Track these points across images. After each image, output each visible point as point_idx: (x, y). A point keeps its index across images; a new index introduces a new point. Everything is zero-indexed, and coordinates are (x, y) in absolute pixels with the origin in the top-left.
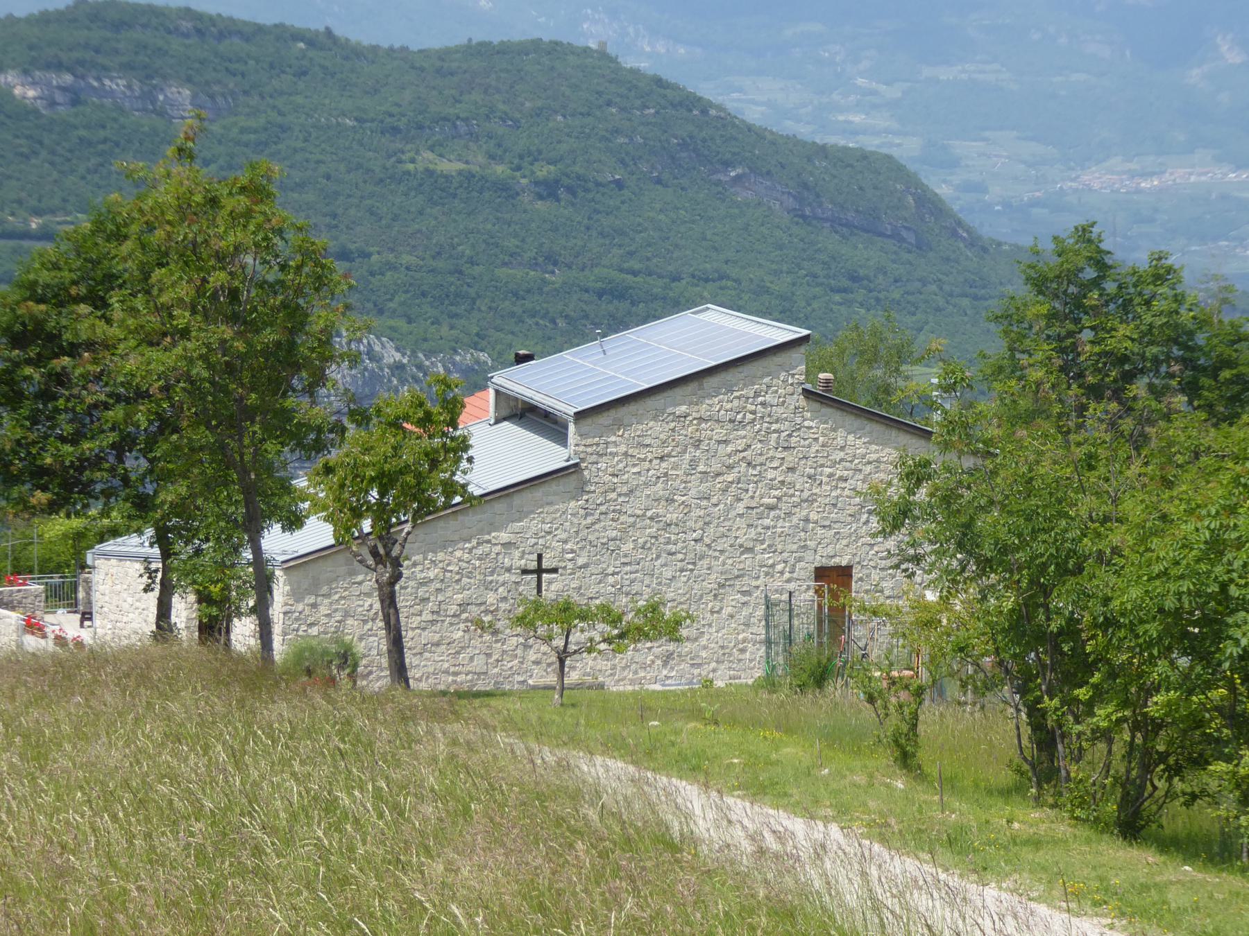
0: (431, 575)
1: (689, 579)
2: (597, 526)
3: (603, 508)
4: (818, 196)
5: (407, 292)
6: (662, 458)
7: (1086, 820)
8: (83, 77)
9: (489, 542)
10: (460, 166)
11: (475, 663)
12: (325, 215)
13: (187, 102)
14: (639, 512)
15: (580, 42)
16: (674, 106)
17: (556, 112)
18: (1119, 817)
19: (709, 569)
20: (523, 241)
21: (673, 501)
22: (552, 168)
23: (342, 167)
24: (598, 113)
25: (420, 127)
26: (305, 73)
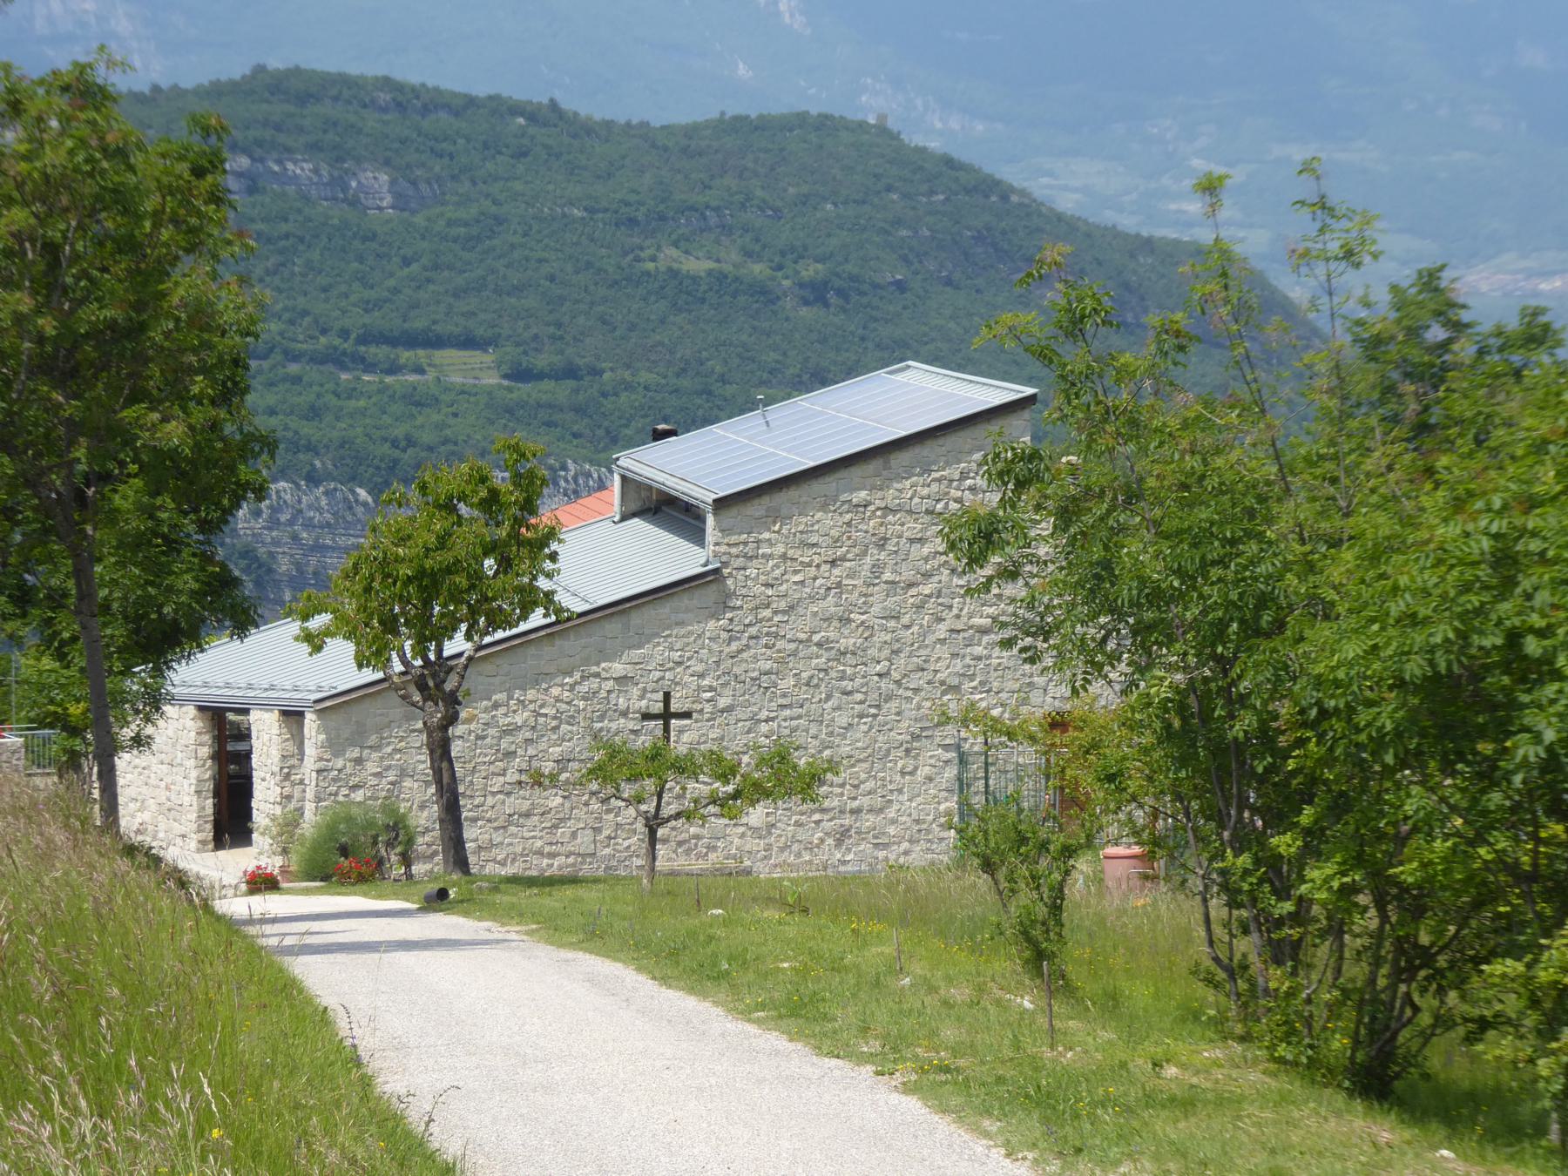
0: (519, 720)
1: (871, 727)
2: (745, 655)
3: (753, 631)
4: (1143, 299)
5: (646, 416)
6: (833, 563)
7: (1296, 1064)
8: (262, 160)
9: (597, 675)
10: (711, 265)
11: (579, 840)
12: (548, 324)
13: (385, 189)
14: (803, 636)
15: (853, 115)
16: (968, 191)
17: (825, 199)
18: (1352, 1058)
19: (898, 714)
20: (785, 354)
21: (849, 620)
22: (820, 266)
23: (569, 268)
24: (876, 200)
25: (662, 218)
26: (525, 154)
